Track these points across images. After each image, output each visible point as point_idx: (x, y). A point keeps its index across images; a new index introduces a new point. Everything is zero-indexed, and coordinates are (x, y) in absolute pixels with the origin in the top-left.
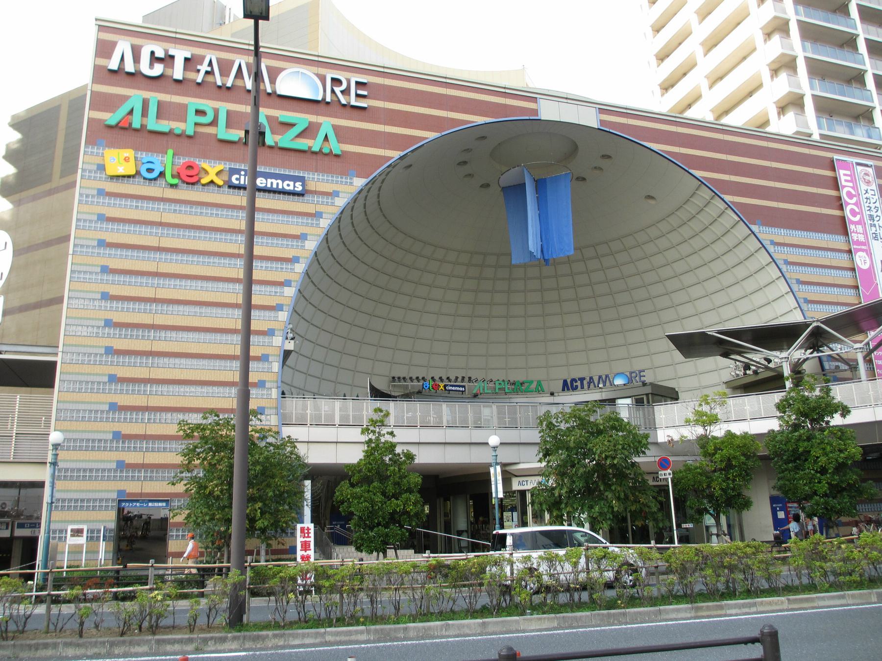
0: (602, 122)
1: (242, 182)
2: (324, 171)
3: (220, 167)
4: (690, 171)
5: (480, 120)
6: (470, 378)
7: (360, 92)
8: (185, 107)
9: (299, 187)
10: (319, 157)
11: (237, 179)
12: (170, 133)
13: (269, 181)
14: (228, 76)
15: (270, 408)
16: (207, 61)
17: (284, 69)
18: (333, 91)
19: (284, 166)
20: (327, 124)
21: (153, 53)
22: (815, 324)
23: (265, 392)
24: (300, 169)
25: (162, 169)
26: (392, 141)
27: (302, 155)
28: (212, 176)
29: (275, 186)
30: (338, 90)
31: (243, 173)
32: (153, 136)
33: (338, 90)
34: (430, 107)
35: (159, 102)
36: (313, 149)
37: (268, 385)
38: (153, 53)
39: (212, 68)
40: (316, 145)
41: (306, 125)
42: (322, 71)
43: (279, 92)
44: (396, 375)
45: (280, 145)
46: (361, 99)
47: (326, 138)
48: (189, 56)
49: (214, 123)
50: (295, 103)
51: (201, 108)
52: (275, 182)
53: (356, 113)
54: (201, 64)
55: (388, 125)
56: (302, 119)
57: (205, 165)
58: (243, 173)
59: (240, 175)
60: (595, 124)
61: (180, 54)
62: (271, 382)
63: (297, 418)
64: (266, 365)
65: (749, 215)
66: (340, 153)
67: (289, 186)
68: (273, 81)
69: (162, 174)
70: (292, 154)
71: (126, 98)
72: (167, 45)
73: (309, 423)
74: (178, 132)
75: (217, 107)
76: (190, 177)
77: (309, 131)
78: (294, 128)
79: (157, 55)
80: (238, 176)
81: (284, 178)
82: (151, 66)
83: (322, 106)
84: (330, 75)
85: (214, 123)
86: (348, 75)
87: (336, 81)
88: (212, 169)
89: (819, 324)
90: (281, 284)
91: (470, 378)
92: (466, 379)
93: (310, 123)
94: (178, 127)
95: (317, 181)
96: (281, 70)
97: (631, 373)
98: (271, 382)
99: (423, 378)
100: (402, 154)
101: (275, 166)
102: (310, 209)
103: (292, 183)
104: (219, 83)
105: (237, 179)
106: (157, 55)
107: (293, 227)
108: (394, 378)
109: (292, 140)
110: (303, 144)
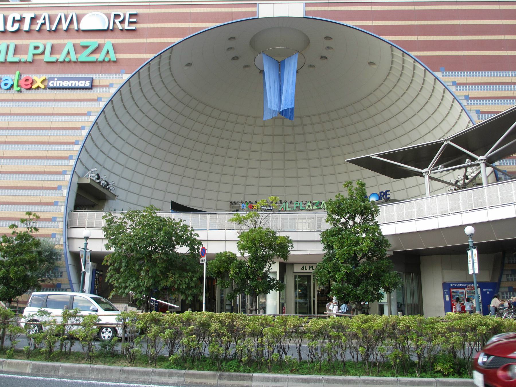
0: (307, 12)
1: (55, 85)
2: (105, 72)
3: (43, 77)
4: (381, 37)
5: (212, 25)
6: (281, 201)
7: (131, 20)
8: (28, 46)
9: (88, 84)
10: (103, 64)
11: (52, 83)
12: (19, 62)
13: (71, 82)
14: (53, 24)
15: (60, 218)
16: (42, 18)
17: (86, 14)
18: (114, 23)
19: (71, 73)
20: (108, 43)
21: (14, 18)
22: (445, 143)
23: (58, 207)
24: (91, 73)
25: (12, 83)
26: (150, 48)
27: (93, 64)
28: (38, 84)
29: (73, 85)
30: (117, 21)
31: (56, 79)
32: (50, 65)
33: (117, 21)
34: (178, 22)
35: (113, 44)
36: (59, 60)
37: (59, 204)
38: (14, 18)
39: (45, 22)
40: (100, 57)
41: (97, 45)
42: (106, 11)
43: (81, 29)
44: (233, 201)
45: (79, 60)
46: (132, 25)
47: (108, 52)
48: (33, 16)
49: (43, 53)
50: (97, 34)
51: (36, 45)
52: (74, 82)
53: (129, 33)
54: (39, 19)
55: (149, 38)
56: (93, 42)
57: (35, 77)
58: (56, 79)
59: (54, 81)
60: (301, 15)
61: (28, 16)
62: (62, 202)
63: (96, 224)
64: (60, 192)
65: (433, 64)
66: (115, 60)
67: (81, 84)
68: (78, 23)
69: (12, 86)
70: (87, 64)
71: (65, 45)
72: (21, 12)
73: (86, 227)
74: (23, 60)
75: (45, 43)
76: (30, 86)
77: (97, 50)
78: (89, 48)
79: (16, 19)
80: (52, 82)
81: (79, 79)
82: (13, 26)
83: (109, 34)
84: (113, 12)
85: (43, 53)
86: (124, 11)
87: (117, 16)
88: (38, 79)
89: (449, 142)
90: (73, 143)
91: (281, 201)
92: (279, 202)
93: (99, 45)
94: (23, 58)
95: (99, 78)
96: (84, 15)
97: (381, 193)
98: (62, 202)
99: (250, 202)
100: (156, 55)
101: (76, 73)
102: (95, 97)
103: (83, 82)
104: (120, 28)
105: (52, 83)
106: (16, 19)
107: (84, 107)
108: (231, 202)
109: (88, 56)
110: (93, 58)
